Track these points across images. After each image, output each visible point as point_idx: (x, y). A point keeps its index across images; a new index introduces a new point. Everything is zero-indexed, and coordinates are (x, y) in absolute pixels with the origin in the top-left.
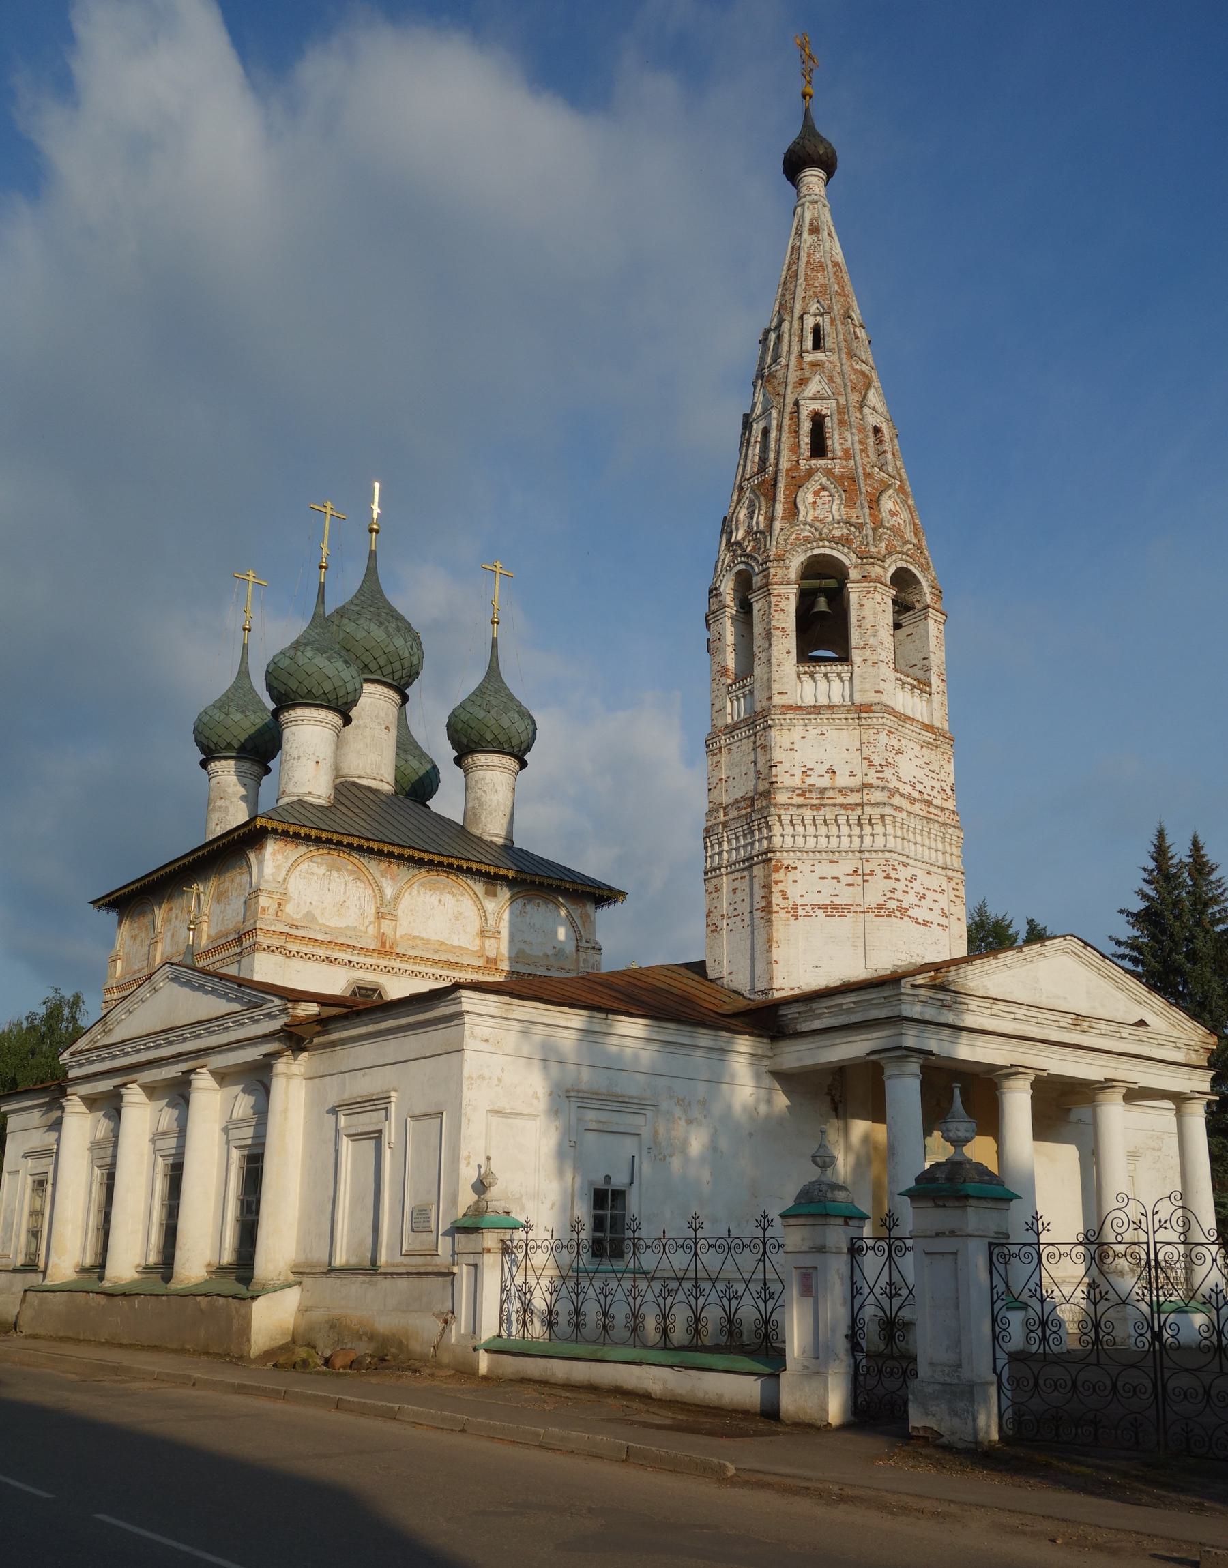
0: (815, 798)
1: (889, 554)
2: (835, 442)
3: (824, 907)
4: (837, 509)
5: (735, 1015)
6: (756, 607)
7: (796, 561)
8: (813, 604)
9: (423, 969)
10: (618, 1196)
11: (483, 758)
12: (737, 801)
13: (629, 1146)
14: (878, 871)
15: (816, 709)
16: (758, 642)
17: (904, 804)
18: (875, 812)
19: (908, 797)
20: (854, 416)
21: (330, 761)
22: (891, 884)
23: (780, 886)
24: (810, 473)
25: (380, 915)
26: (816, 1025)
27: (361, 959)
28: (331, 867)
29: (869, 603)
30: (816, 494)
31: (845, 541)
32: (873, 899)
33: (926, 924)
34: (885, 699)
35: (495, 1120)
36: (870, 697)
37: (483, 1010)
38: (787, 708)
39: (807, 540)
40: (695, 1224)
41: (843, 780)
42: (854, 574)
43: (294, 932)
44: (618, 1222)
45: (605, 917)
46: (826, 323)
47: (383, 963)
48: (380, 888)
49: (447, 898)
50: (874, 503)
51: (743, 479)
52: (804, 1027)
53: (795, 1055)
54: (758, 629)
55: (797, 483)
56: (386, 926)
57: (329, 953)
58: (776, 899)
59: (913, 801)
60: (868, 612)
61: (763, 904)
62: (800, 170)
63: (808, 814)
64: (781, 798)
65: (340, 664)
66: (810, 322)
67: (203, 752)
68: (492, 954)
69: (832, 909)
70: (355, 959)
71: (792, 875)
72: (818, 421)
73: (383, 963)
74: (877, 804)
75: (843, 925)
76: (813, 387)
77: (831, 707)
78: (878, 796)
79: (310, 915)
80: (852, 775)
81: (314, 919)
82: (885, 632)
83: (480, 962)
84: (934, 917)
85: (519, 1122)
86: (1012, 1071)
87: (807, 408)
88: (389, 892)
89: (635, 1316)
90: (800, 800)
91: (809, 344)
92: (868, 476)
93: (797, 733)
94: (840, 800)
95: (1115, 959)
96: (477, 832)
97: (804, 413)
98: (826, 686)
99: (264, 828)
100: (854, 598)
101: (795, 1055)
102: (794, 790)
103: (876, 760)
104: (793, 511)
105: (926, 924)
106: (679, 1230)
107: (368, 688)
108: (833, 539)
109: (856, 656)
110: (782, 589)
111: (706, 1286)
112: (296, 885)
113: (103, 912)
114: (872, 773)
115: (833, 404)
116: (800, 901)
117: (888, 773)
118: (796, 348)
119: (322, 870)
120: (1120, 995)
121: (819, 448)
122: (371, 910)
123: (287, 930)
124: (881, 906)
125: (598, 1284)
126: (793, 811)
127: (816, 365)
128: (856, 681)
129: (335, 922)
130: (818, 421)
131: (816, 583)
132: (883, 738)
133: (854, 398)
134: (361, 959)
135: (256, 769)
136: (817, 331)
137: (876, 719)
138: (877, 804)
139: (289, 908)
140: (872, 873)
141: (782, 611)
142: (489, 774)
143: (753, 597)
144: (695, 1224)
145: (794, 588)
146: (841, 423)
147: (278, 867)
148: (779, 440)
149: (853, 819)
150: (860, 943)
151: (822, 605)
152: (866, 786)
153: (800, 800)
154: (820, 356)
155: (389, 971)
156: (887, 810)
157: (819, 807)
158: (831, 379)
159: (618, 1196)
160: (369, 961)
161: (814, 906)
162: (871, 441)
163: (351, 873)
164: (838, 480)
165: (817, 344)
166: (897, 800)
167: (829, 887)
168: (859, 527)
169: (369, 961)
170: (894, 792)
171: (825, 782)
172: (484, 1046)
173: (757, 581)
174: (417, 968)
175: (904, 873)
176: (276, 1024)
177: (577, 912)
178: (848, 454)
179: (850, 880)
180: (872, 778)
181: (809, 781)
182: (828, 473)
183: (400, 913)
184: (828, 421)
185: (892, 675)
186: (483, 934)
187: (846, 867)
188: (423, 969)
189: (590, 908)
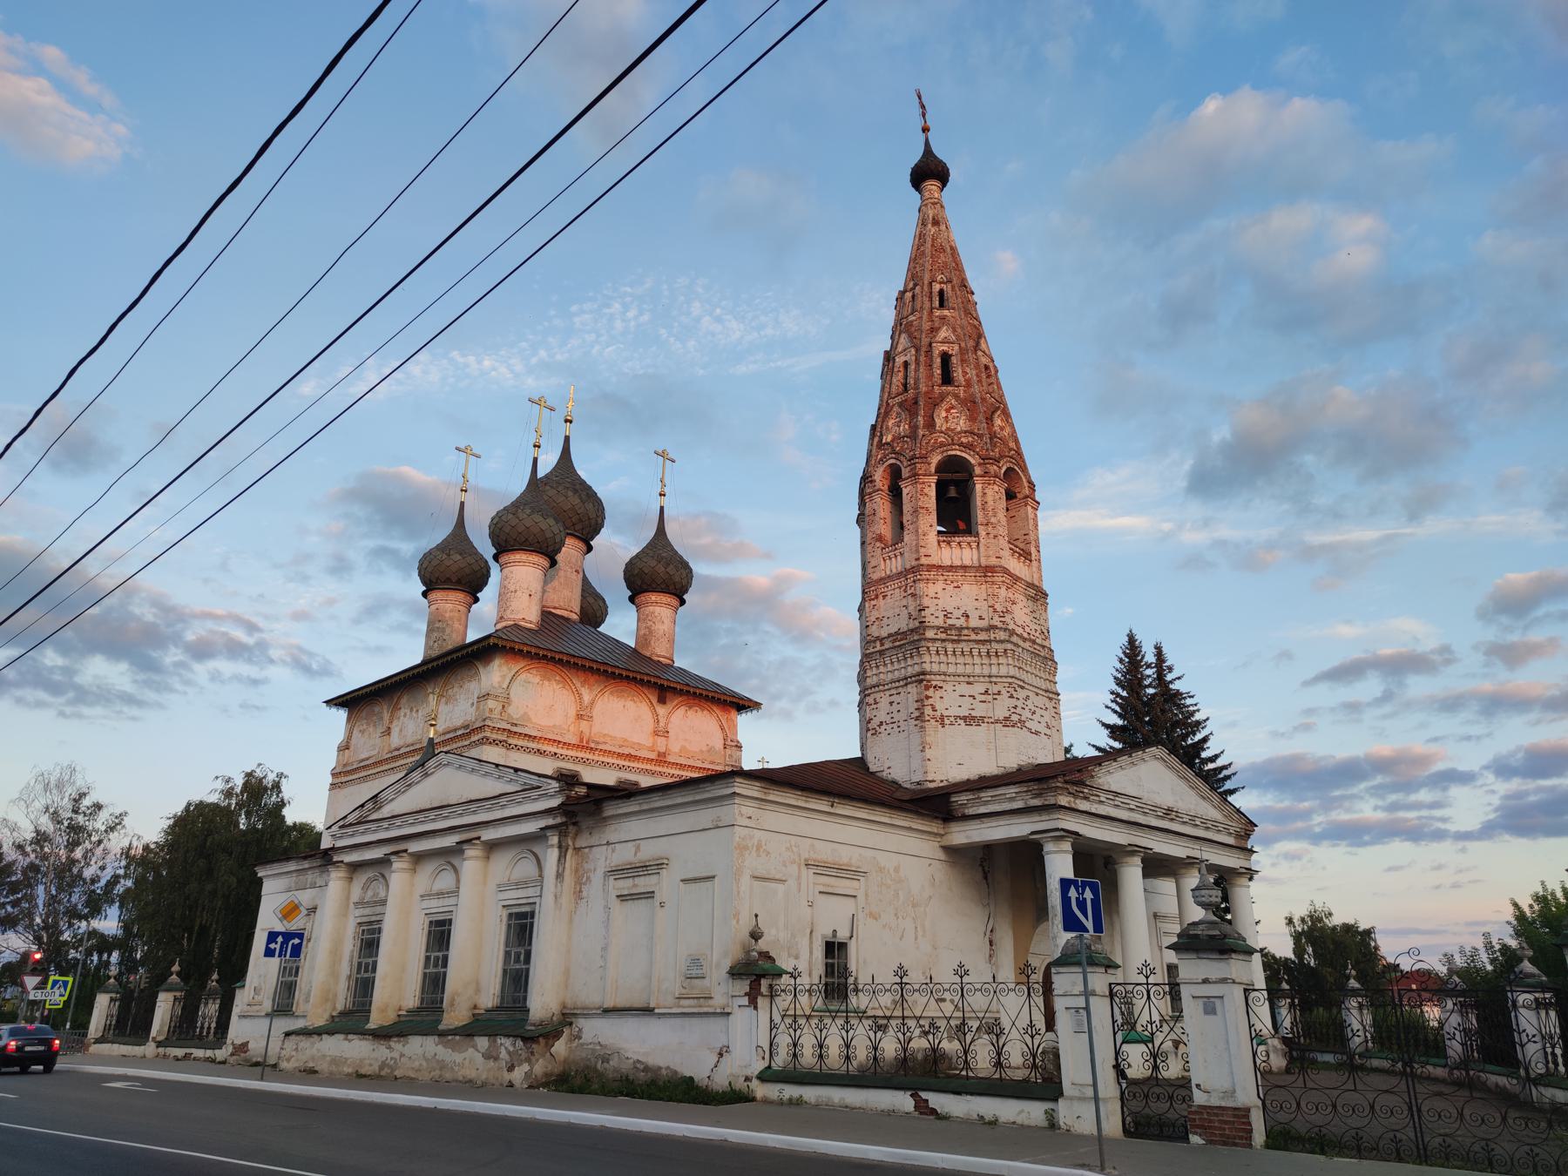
0: (954, 634)
1: (1002, 457)
2: (958, 374)
3: (964, 718)
4: (962, 424)
5: (910, 801)
6: (905, 491)
7: (935, 459)
8: (947, 491)
9: (610, 760)
10: (843, 946)
11: (653, 597)
12: (890, 635)
13: (848, 907)
14: (1004, 692)
15: (951, 568)
16: (906, 518)
17: (1021, 643)
18: (1000, 648)
19: (1020, 636)
20: (971, 356)
21: (539, 595)
22: (1013, 702)
23: (930, 701)
24: (942, 397)
25: (580, 717)
26: (983, 810)
27: (565, 752)
28: (544, 678)
29: (989, 492)
30: (947, 411)
31: (969, 447)
32: (1001, 713)
33: (1037, 733)
34: (1003, 563)
35: (756, 883)
36: (993, 561)
37: (749, 793)
38: (931, 567)
39: (942, 445)
40: (901, 972)
41: (974, 623)
42: (978, 470)
43: (514, 729)
44: (845, 972)
45: (744, 721)
46: (947, 288)
47: (581, 755)
48: (580, 695)
49: (630, 704)
50: (990, 420)
51: (890, 397)
52: (971, 811)
53: (964, 834)
54: (907, 507)
55: (935, 403)
56: (584, 725)
57: (540, 746)
58: (928, 711)
59: (1025, 640)
60: (989, 499)
61: (917, 714)
62: (924, 180)
63: (950, 647)
64: (930, 634)
65: (551, 521)
66: (936, 287)
67: (424, 583)
68: (663, 750)
69: (969, 720)
70: (559, 751)
71: (939, 693)
72: (946, 358)
73: (581, 755)
74: (1002, 642)
75: (981, 732)
76: (944, 333)
77: (964, 568)
78: (1002, 635)
79: (525, 716)
80: (981, 618)
81: (529, 719)
82: (1001, 515)
83: (653, 756)
84: (1042, 728)
85: (773, 885)
86: (1130, 850)
87: (939, 348)
88: (587, 698)
89: (795, 1045)
90: (943, 636)
91: (937, 304)
92: (983, 399)
93: (940, 585)
94: (973, 637)
95: (534, 781)
96: (648, 654)
97: (936, 353)
98: (951, 554)
99: (496, 645)
100: (978, 487)
101: (964, 834)
102: (938, 628)
103: (999, 607)
104: (930, 424)
105: (1037, 733)
106: (887, 978)
107: (569, 541)
108: (961, 444)
109: (982, 531)
110: (926, 479)
111: (911, 1023)
112: (517, 692)
113: (334, 710)
114: (996, 618)
115: (956, 347)
116: (946, 713)
117: (1008, 618)
118: (927, 305)
119: (537, 679)
120: (1192, 792)
121: (947, 379)
122: (572, 713)
123: (508, 727)
124: (1006, 719)
125: (840, 1022)
126: (938, 644)
127: (943, 318)
128: (982, 548)
129: (545, 722)
130: (946, 358)
131: (948, 476)
132: (1003, 592)
133: (971, 343)
134: (565, 752)
135: (469, 599)
136: (941, 293)
137: (998, 578)
138: (1002, 642)
139: (511, 710)
140: (999, 693)
141: (924, 495)
142: (658, 609)
143: (902, 484)
144: (901, 972)
145: (934, 479)
146: (963, 361)
147: (504, 677)
148: (916, 370)
149: (984, 650)
150: (992, 746)
151: (952, 492)
152: (994, 627)
153: (943, 636)
154: (946, 312)
155: (584, 762)
156: (1009, 646)
157: (958, 641)
158: (954, 330)
159: (843, 946)
160: (570, 753)
161: (956, 717)
162: (984, 376)
163: (558, 682)
164: (963, 402)
165: (942, 305)
166: (1015, 639)
167: (967, 701)
168: (980, 436)
169: (570, 753)
170: (1012, 633)
171: (961, 622)
172: (746, 822)
173: (905, 473)
174: (606, 760)
175: (1022, 694)
176: (555, 802)
177: (723, 717)
178: (969, 384)
179: (983, 698)
180: (996, 622)
181: (949, 622)
182: (956, 396)
183: (1059, 688)
184: (954, 360)
185: (1007, 546)
186: (656, 733)
187: (979, 688)
188: (610, 760)
189: (734, 713)
